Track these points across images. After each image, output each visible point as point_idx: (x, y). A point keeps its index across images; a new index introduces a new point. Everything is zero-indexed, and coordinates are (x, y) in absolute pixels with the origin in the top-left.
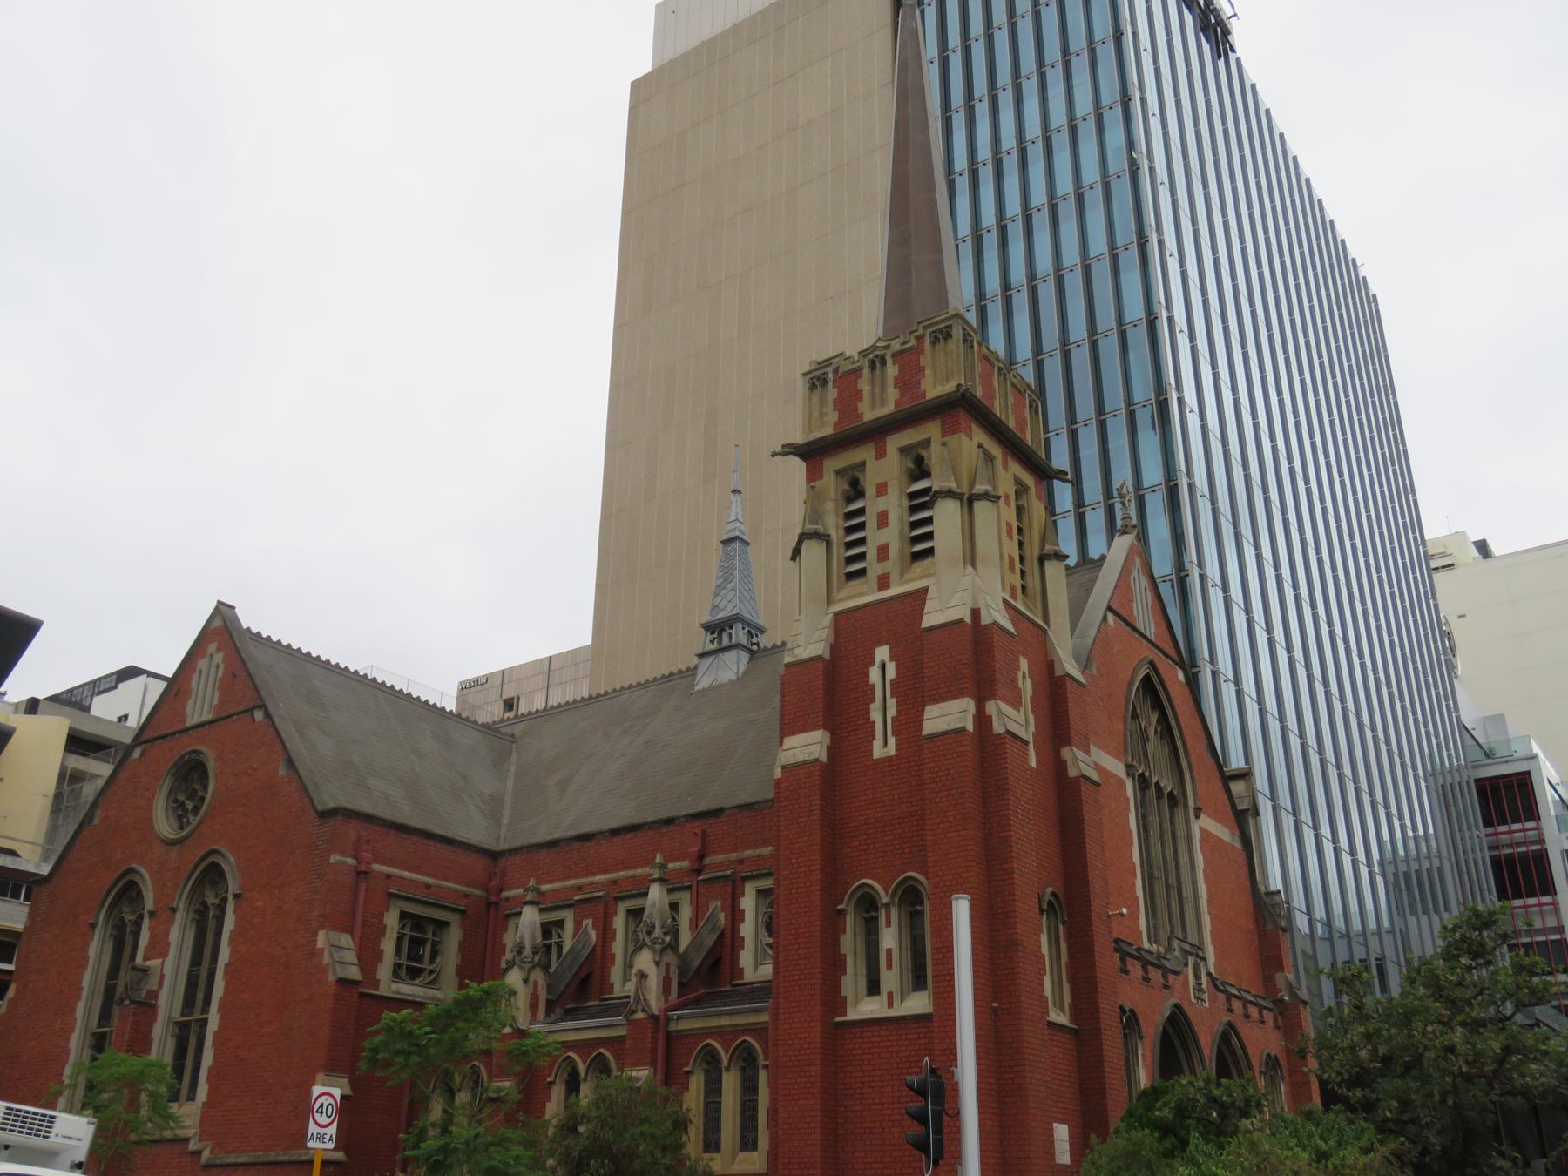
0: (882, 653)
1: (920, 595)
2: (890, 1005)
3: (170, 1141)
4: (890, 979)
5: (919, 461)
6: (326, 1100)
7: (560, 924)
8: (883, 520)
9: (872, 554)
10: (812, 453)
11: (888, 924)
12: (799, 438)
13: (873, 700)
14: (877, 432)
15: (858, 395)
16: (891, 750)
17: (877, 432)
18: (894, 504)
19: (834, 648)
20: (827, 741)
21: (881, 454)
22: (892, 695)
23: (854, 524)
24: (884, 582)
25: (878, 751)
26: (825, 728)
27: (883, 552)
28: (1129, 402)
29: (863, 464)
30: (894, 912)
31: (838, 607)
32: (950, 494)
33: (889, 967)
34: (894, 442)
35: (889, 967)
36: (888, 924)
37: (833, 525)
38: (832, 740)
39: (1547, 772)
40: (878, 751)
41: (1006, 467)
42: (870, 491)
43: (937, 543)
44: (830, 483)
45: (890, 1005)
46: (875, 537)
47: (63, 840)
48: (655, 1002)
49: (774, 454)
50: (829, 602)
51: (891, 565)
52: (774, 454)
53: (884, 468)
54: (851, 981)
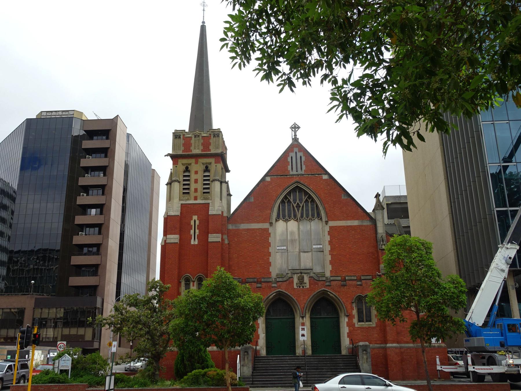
0: (195, 217)
3: (47, 342)
5: (207, 167)
6: (62, 345)
7: (16, 383)
8: (196, 181)
10: (173, 157)
11: (193, 285)
12: (171, 152)
13: (198, 226)
14: (197, 157)
15: (190, 145)
16: (196, 243)
18: (200, 177)
21: (196, 163)
23: (187, 179)
24: (196, 198)
27: (196, 190)
28: (221, 200)
29: (191, 164)
30: (195, 283)
34: (202, 161)
36: (193, 285)
39: (433, 246)
40: (192, 242)
44: (182, 168)
51: (199, 194)
53: (197, 167)
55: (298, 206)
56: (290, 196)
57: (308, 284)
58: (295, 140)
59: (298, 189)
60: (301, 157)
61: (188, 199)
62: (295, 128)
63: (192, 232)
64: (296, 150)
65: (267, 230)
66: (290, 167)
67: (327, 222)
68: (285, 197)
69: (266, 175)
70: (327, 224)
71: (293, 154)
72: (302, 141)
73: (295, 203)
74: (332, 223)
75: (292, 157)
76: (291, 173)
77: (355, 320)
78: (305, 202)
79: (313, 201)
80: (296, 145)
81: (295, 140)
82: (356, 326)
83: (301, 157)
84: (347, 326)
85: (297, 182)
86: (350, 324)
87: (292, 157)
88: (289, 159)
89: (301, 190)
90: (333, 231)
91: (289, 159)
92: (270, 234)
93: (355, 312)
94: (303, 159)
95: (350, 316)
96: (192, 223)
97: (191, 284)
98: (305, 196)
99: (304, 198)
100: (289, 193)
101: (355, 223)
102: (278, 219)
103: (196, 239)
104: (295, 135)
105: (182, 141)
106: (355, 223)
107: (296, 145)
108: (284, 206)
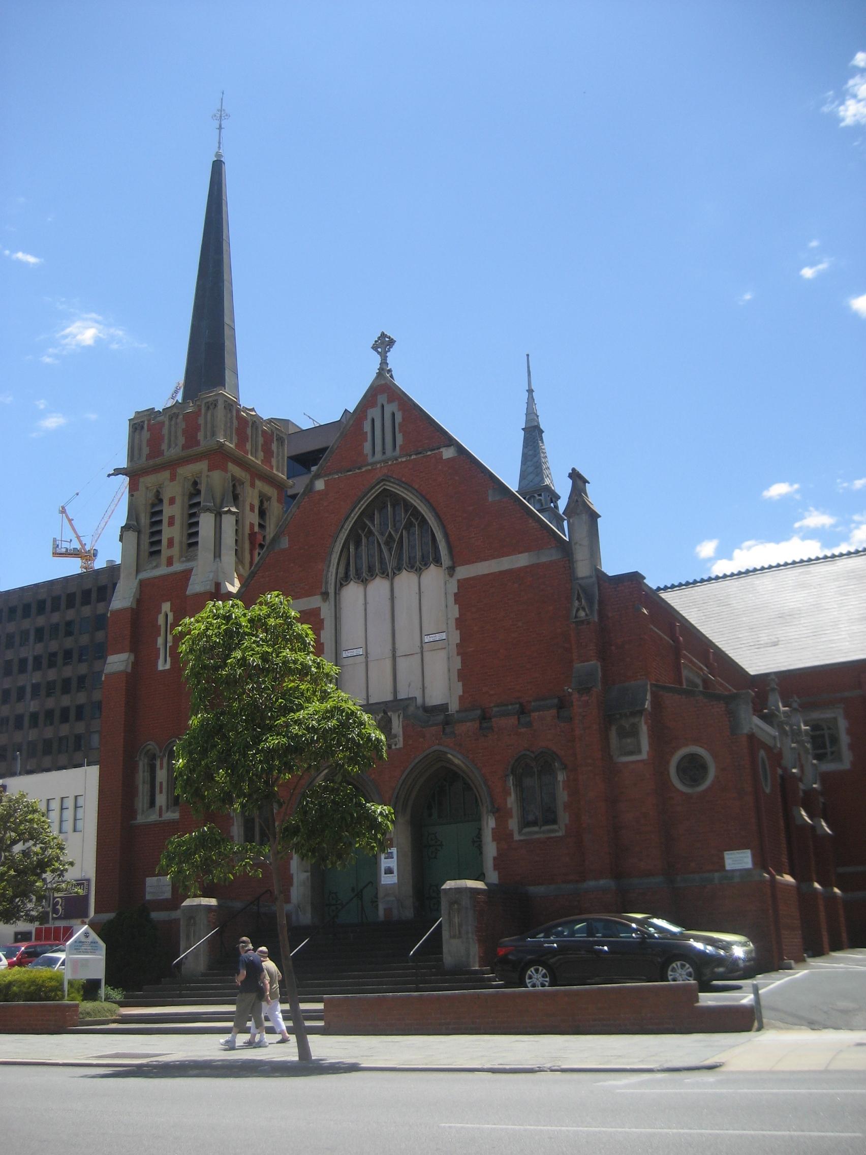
1: (186, 575)
2: (160, 816)
4: (161, 799)
9: (165, 542)
11: (161, 768)
16: (168, 666)
17: (172, 465)
19: (139, 601)
20: (132, 658)
22: (400, 432)
24: (170, 562)
25: (161, 667)
26: (131, 651)
27: (171, 543)
31: (144, 575)
32: (208, 510)
33: (161, 792)
35: (161, 792)
37: (145, 520)
38: (135, 657)
40: (161, 667)
41: (253, 485)
42: (166, 502)
43: (200, 539)
45: (160, 816)
46: (167, 532)
47: (781, 1025)
48: (383, 856)
49: (109, 475)
50: (138, 571)
51: (175, 551)
52: (109, 475)
54: (141, 801)
55: (390, 540)
56: (372, 521)
57: (401, 739)
58: (384, 371)
59: (385, 500)
60: (393, 414)
61: (157, 567)
62: (384, 344)
63: (160, 641)
64: (382, 399)
65: (86, 915)
66: (367, 446)
67: (451, 570)
68: (359, 524)
69: (461, 450)
70: (451, 576)
71: (374, 413)
72: (404, 381)
73: (382, 534)
74: (464, 572)
75: (373, 420)
76: (370, 460)
77: (513, 824)
78: (405, 528)
79: (423, 521)
80: (383, 390)
81: (384, 371)
82: (517, 837)
83: (393, 414)
84: (494, 839)
85: (383, 480)
86: (501, 835)
87: (373, 420)
88: (367, 427)
89: (397, 501)
90: (468, 596)
91: (367, 427)
92: (322, 621)
93: (512, 801)
94: (399, 418)
95: (500, 812)
96: (161, 620)
97: (158, 763)
98: (406, 511)
99: (403, 517)
100: (368, 513)
101: (521, 560)
102: (344, 580)
103: (168, 659)
104: (384, 362)
105: (146, 435)
106: (521, 560)
107: (383, 390)
108: (358, 544)
